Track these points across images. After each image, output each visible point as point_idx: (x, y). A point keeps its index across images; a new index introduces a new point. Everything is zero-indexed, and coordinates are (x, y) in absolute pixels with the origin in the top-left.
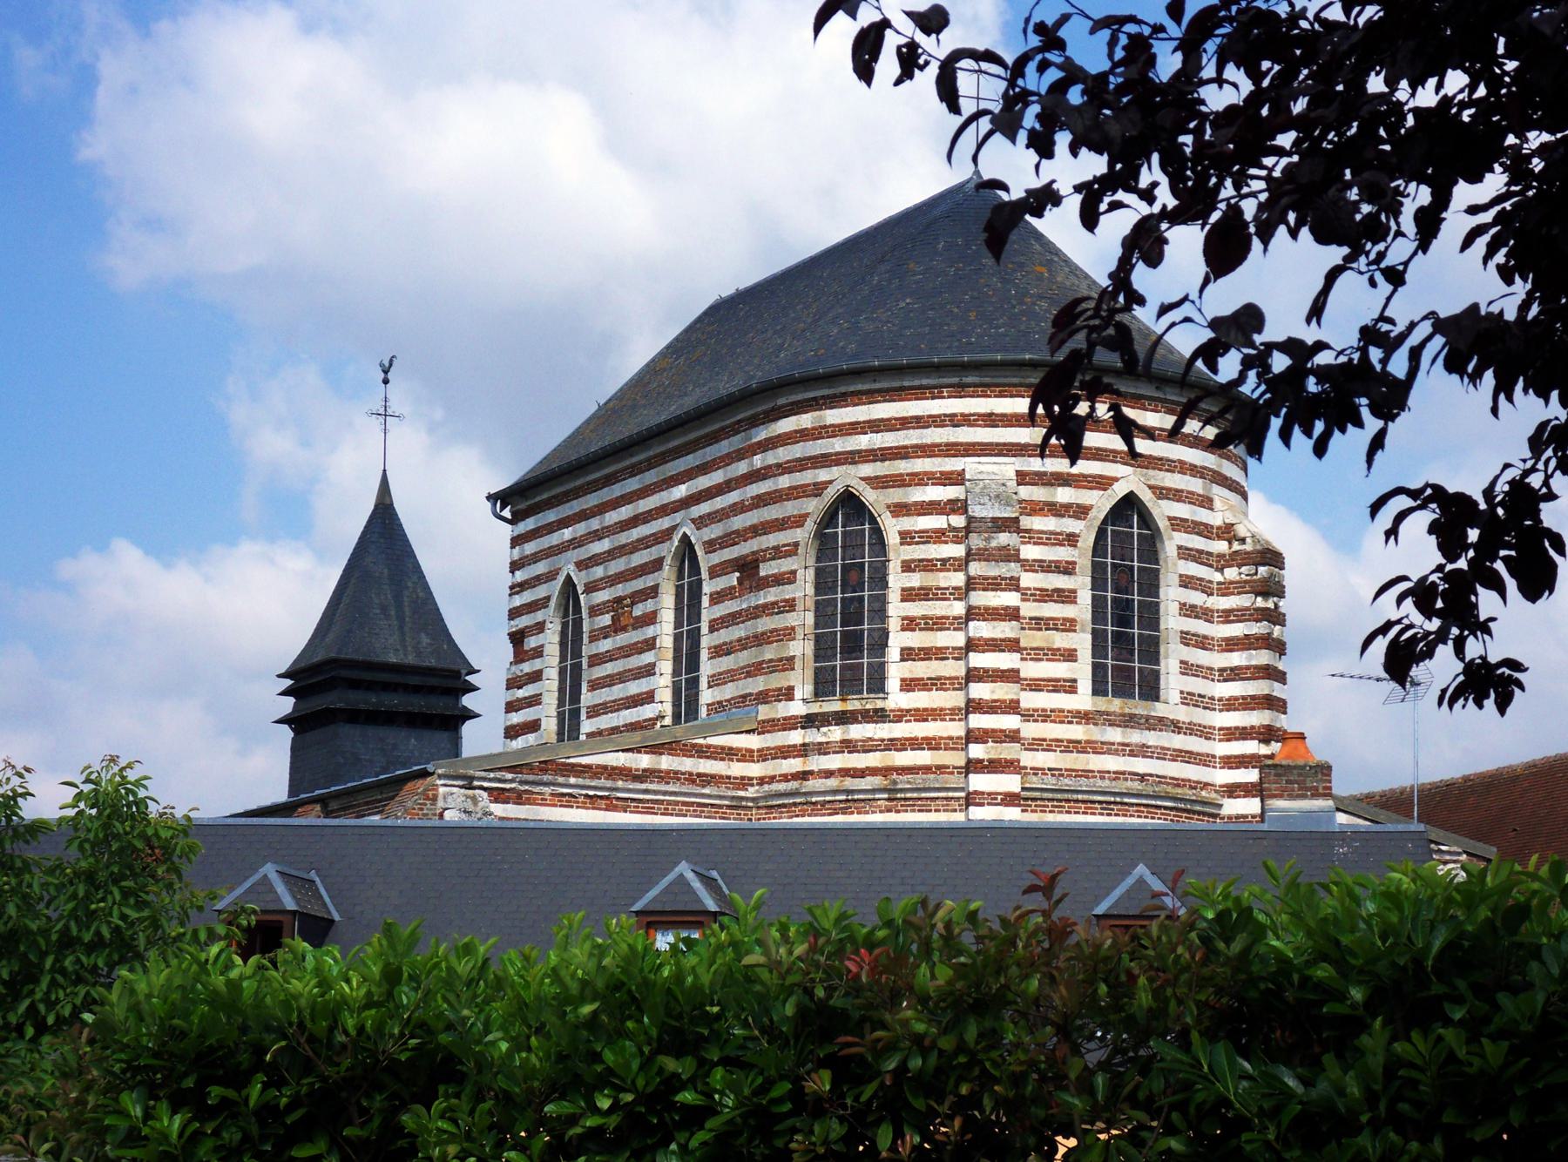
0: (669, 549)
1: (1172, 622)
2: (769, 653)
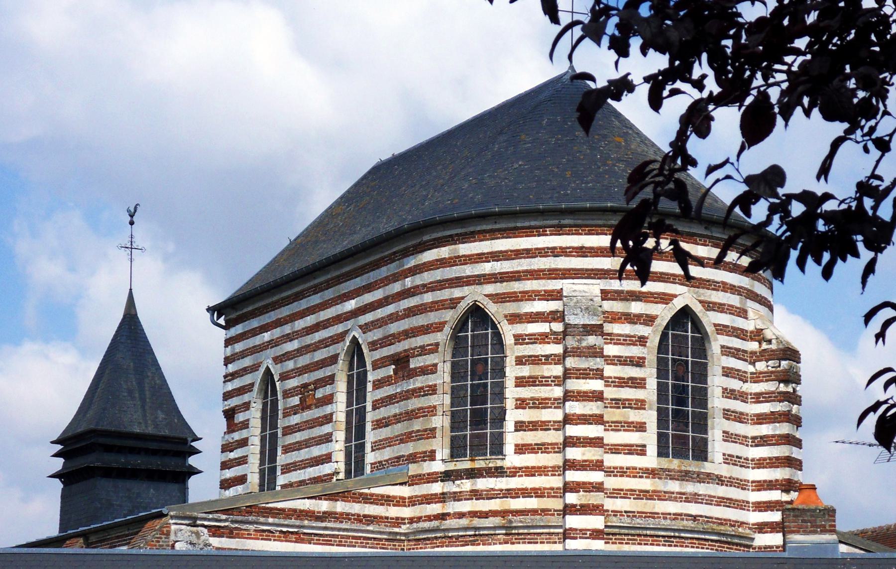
1: (717, 402)
2: (417, 425)
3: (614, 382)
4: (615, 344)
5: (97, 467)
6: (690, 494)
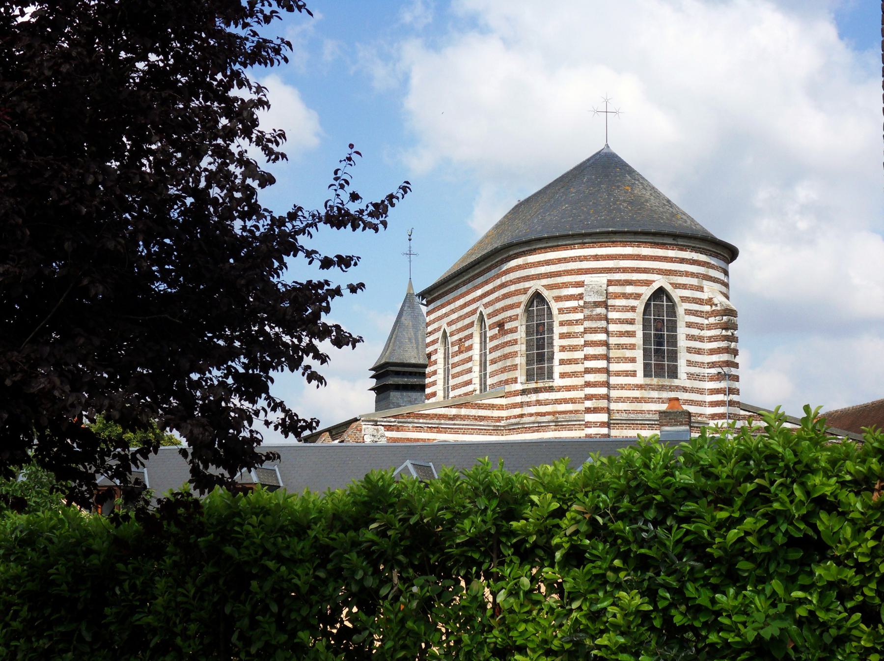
1: (682, 343)
2: (509, 362)
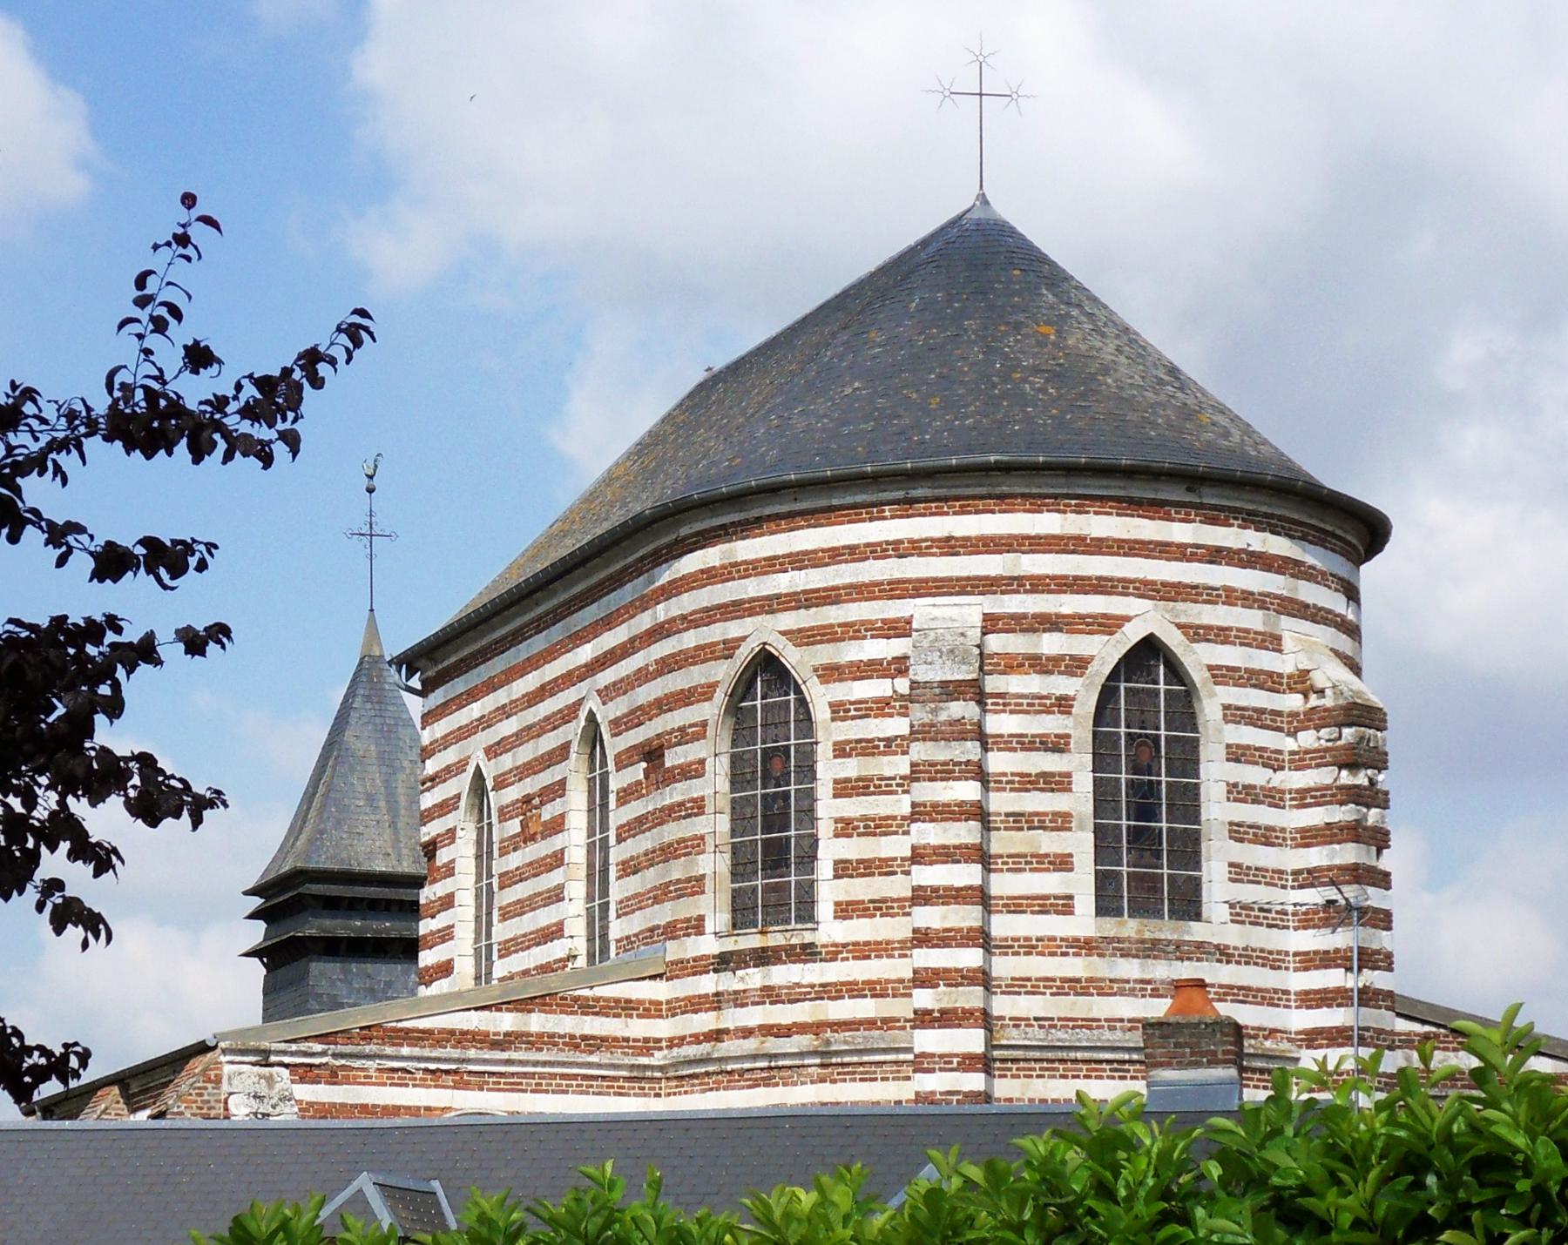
0: (573, 731)
1: (1216, 809)
3: (1012, 782)
4: (1012, 712)
5: (311, 938)
6: (1162, 982)
